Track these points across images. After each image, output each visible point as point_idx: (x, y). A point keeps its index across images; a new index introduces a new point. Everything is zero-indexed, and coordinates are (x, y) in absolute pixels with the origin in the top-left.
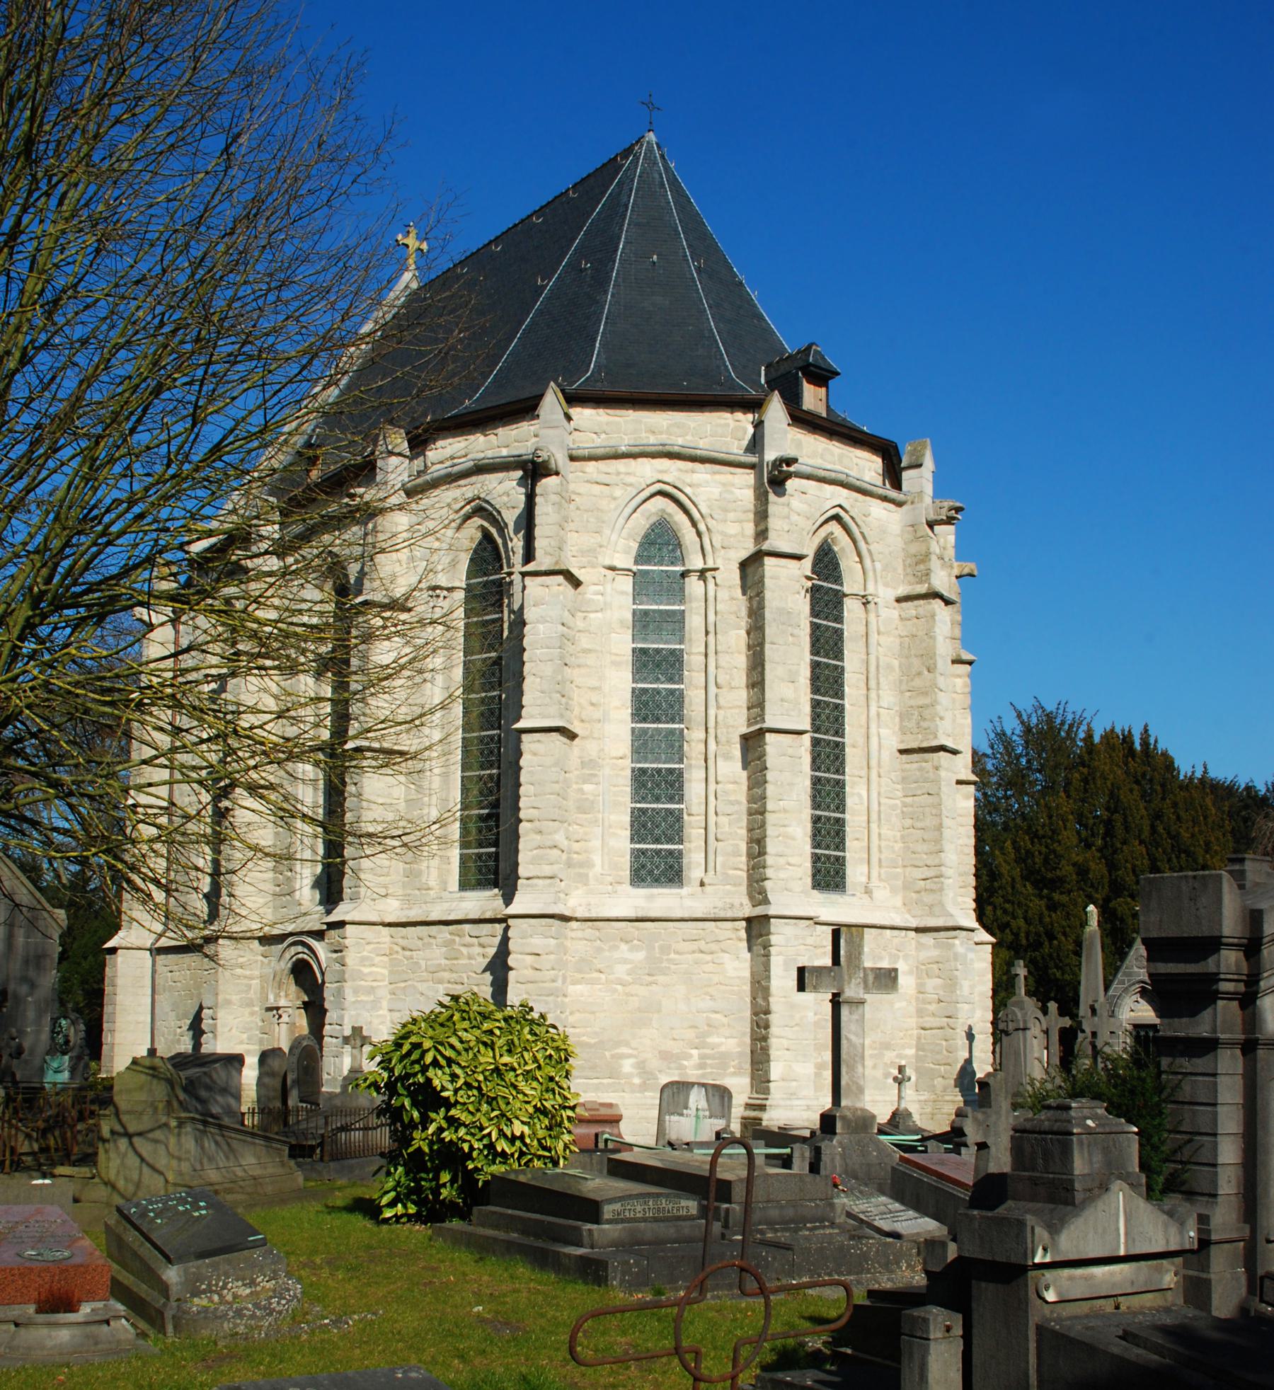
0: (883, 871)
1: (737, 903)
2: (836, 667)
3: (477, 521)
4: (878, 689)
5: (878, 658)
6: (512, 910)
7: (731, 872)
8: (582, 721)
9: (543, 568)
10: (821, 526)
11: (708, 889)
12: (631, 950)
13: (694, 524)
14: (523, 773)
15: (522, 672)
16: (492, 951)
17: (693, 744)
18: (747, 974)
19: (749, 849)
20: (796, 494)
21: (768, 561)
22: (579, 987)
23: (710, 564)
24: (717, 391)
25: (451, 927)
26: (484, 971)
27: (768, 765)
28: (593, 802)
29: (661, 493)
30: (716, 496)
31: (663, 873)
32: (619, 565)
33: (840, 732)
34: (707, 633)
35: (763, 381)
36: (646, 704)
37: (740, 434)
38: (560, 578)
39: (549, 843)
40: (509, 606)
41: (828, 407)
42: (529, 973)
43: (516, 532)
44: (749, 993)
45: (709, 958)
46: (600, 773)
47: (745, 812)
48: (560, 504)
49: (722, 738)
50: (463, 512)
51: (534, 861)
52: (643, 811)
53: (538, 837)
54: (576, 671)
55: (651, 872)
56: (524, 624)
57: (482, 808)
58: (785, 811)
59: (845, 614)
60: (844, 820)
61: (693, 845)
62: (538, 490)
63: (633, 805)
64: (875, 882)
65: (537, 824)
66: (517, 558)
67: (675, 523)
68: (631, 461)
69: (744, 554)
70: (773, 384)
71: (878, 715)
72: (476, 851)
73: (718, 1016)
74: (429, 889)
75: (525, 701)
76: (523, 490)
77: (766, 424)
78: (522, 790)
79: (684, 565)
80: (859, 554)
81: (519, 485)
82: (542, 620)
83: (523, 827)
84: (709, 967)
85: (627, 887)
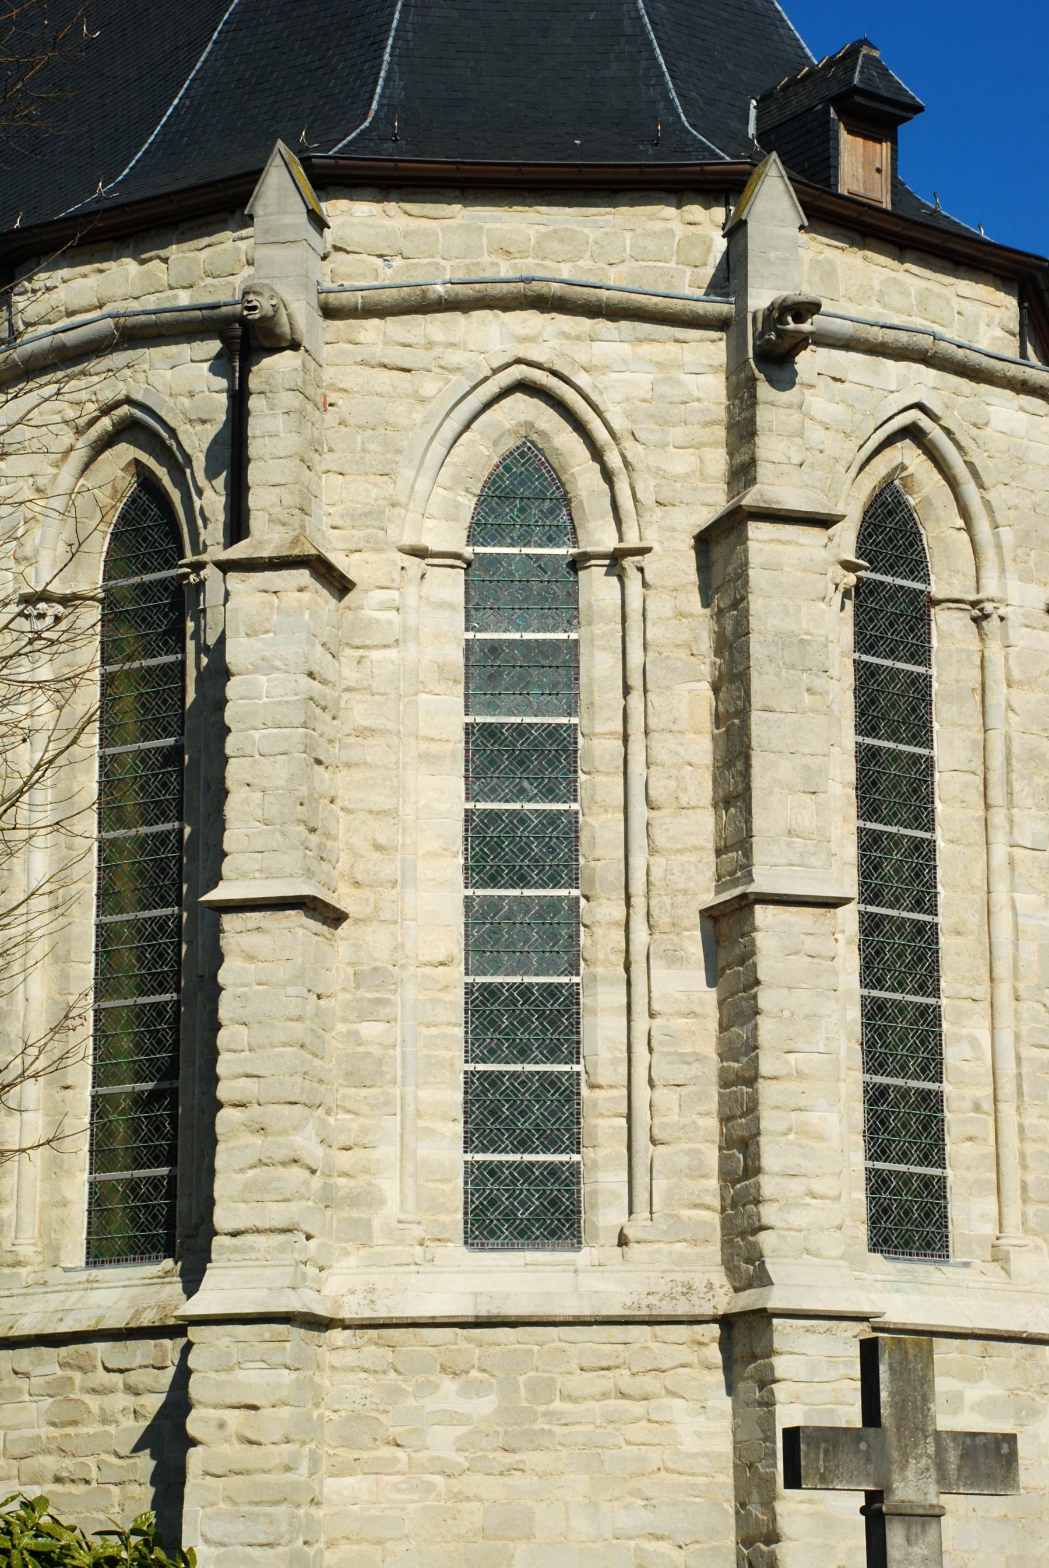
0: (1031, 1209)
1: (699, 1282)
2: (916, 759)
3: (125, 452)
4: (1010, 805)
5: (1008, 739)
6: (201, 1304)
7: (686, 1213)
8: (357, 884)
9: (266, 553)
10: (877, 451)
11: (634, 1250)
12: (464, 1392)
13: (597, 453)
14: (224, 999)
15: (223, 779)
16: (153, 1403)
17: (599, 931)
18: (725, 1446)
19: (723, 1160)
20: (820, 382)
21: (758, 532)
22: (348, 1481)
23: (632, 541)
24: (647, 156)
25: (63, 1350)
26: (137, 1449)
27: (761, 975)
28: (380, 1062)
29: (523, 387)
30: (644, 392)
31: (537, 1217)
32: (434, 546)
33: (926, 901)
34: (627, 690)
35: (752, 130)
36: (496, 846)
37: (696, 254)
38: (303, 576)
39: (281, 1155)
40: (195, 636)
41: (896, 186)
42: (234, 1452)
43: (211, 474)
44: (730, 1493)
45: (637, 1408)
46: (396, 998)
47: (714, 1079)
48: (302, 413)
49: (662, 918)
50: (94, 432)
51: (248, 1195)
52: (492, 1080)
53: (258, 1140)
54: (343, 777)
55: (509, 1216)
56: (226, 674)
57: (141, 1079)
58: (801, 1075)
59: (935, 643)
60: (939, 1096)
61: (601, 1153)
62: (254, 382)
63: (470, 1067)
64: (1014, 1234)
65: (254, 1110)
66: (213, 533)
67: (557, 451)
68: (457, 316)
69: (705, 517)
70: (769, 139)
71: (1011, 863)
72: (126, 1174)
73: (662, 1546)
74: (18, 1264)
75: (229, 841)
76: (224, 383)
77: (751, 228)
78: (223, 1038)
79: (575, 543)
80: (964, 512)
81: (213, 370)
82: (266, 666)
83: (225, 1119)
84: (639, 1432)
85: (457, 1250)
